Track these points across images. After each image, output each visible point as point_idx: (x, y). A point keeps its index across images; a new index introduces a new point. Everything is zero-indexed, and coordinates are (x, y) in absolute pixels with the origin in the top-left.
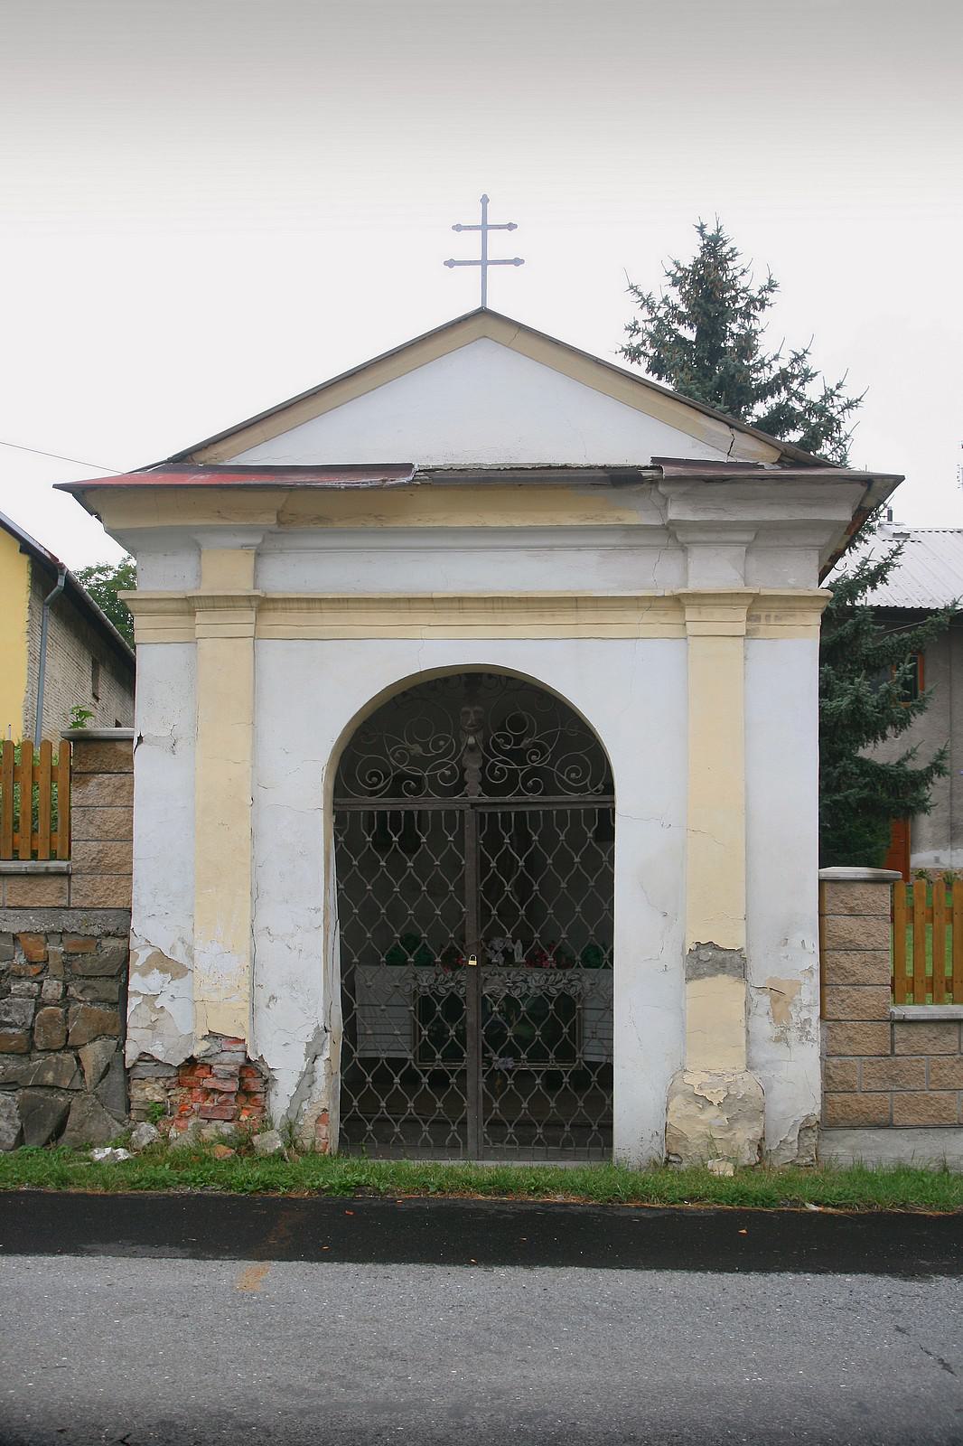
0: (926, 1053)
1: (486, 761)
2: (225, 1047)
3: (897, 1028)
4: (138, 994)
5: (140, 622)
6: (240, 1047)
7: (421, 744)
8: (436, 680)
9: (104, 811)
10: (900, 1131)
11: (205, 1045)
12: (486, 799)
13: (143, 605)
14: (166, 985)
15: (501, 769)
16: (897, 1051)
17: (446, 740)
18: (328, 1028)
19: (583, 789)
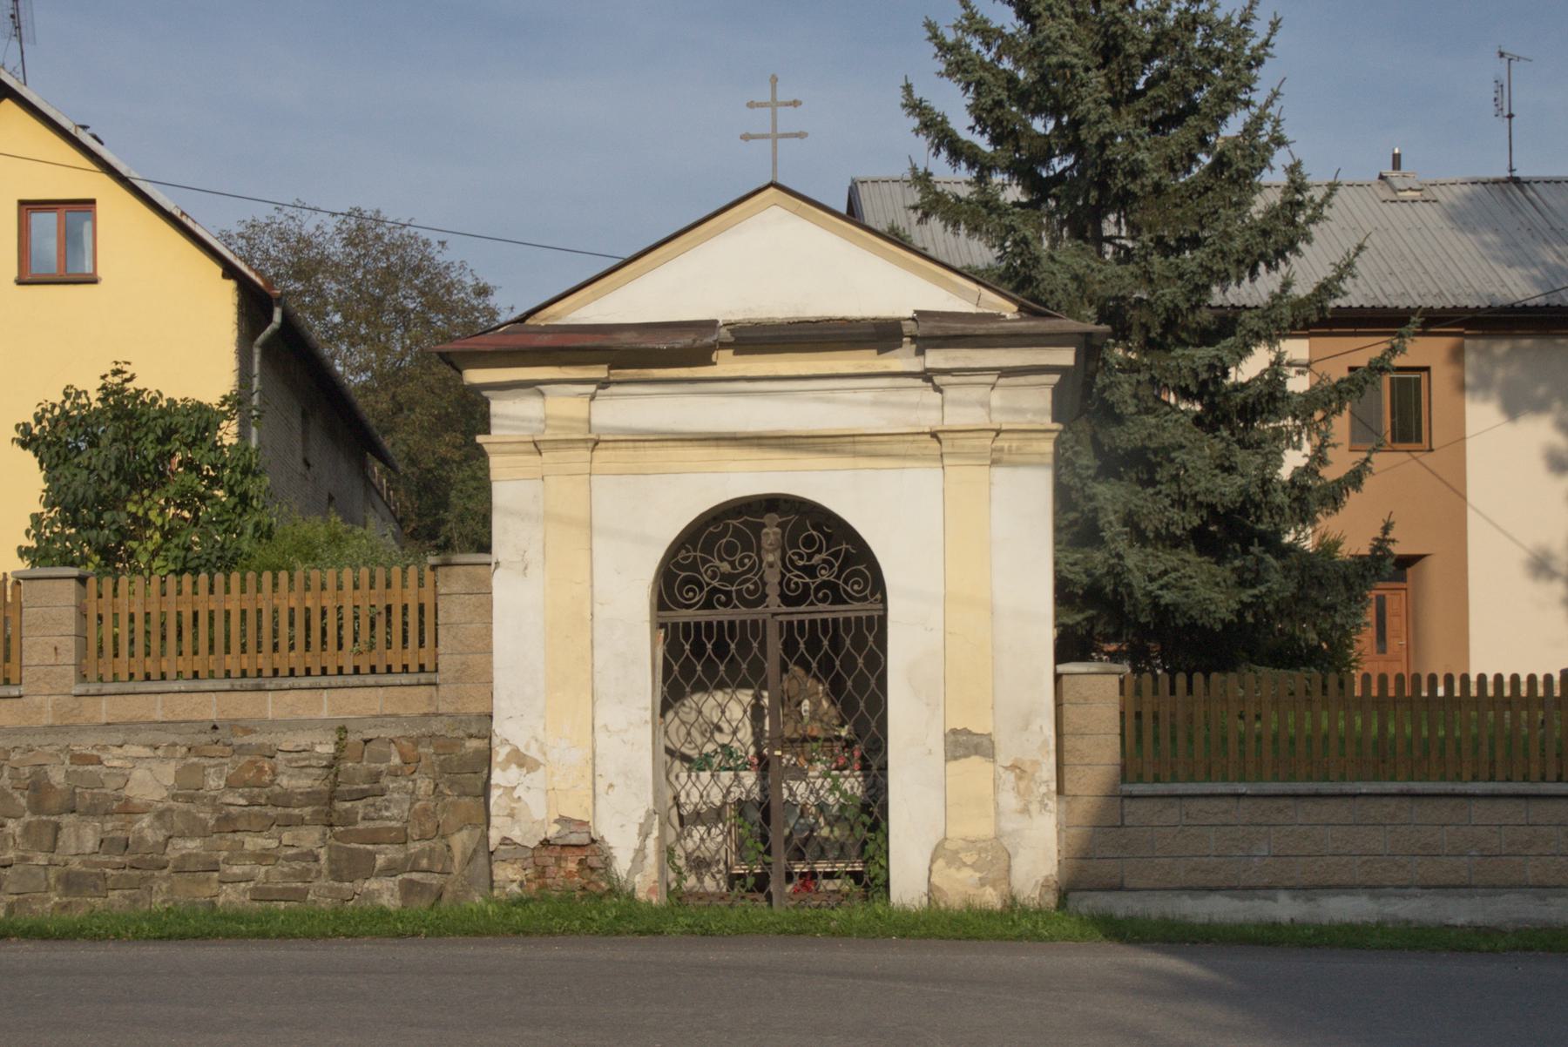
1: (783, 575)
2: (573, 828)
3: (1127, 802)
4: (498, 786)
6: (586, 829)
12: (784, 609)
13: (497, 447)
15: (796, 583)
16: (1126, 823)
17: (750, 557)
19: (865, 599)
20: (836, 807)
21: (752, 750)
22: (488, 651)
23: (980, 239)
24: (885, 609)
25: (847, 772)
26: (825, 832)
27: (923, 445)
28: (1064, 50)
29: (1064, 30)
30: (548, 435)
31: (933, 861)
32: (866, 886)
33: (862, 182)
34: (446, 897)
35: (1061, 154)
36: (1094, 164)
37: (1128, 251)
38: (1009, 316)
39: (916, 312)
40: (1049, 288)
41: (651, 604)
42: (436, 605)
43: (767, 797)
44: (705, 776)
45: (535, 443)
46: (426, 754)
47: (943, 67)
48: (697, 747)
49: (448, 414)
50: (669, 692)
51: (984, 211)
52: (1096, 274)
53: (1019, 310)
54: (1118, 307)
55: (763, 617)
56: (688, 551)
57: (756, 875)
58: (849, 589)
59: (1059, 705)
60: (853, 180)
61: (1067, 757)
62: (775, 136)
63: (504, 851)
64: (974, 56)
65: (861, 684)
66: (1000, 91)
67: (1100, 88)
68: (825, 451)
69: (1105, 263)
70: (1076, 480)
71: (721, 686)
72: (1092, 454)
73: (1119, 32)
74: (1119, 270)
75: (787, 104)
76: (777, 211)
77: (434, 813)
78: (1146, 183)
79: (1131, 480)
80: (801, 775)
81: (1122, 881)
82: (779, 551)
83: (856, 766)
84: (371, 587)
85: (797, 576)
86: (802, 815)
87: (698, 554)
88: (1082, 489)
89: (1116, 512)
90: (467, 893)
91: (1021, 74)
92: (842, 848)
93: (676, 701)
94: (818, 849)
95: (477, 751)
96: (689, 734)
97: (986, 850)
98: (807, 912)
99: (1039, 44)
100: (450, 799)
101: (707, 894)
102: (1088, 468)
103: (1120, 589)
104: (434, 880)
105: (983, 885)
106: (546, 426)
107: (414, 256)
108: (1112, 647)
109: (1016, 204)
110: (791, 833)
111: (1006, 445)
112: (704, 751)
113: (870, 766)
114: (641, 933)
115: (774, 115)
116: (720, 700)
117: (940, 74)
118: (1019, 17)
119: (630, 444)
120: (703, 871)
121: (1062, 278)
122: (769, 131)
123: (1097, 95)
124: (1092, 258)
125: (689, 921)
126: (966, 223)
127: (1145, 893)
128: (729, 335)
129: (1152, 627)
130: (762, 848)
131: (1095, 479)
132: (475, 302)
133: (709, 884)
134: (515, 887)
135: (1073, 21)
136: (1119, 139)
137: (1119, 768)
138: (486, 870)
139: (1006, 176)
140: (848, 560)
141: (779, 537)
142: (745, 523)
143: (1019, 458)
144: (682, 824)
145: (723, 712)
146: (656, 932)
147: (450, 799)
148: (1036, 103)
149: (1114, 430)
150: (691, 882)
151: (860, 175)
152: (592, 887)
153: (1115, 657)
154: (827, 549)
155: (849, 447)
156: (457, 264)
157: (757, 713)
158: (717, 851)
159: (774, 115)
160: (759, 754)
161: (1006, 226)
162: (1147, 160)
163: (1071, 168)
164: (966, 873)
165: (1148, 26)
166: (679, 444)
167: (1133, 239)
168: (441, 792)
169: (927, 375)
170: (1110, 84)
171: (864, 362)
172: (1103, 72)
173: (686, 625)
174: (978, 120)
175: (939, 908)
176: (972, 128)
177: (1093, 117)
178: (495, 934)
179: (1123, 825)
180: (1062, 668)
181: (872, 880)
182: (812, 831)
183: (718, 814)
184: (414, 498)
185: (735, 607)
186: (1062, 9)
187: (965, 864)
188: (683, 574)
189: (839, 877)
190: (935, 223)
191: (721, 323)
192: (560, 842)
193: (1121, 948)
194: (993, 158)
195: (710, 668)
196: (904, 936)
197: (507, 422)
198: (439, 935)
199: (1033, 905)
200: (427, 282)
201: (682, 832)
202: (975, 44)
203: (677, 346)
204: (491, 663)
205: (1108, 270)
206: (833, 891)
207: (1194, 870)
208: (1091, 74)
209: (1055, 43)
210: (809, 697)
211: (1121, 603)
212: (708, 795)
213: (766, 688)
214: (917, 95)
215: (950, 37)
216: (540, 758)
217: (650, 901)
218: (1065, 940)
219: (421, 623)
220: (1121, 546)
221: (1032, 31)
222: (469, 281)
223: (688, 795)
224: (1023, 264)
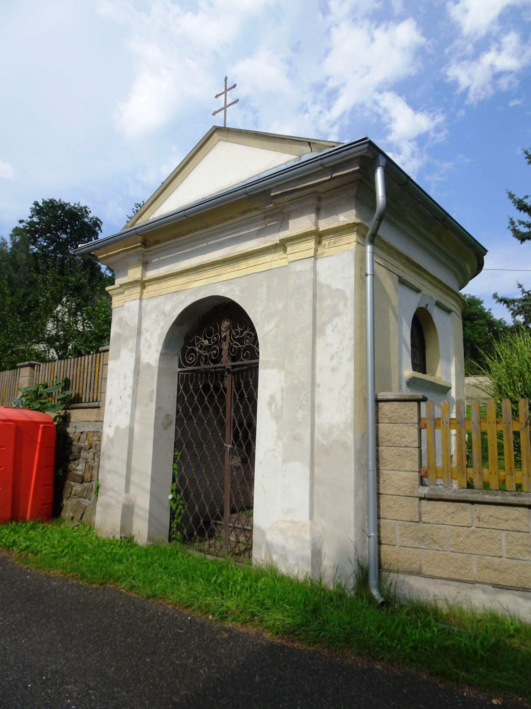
1: (230, 344)
3: (424, 502)
16: (423, 519)
76: (221, 143)
127: (439, 581)
207: (487, 567)
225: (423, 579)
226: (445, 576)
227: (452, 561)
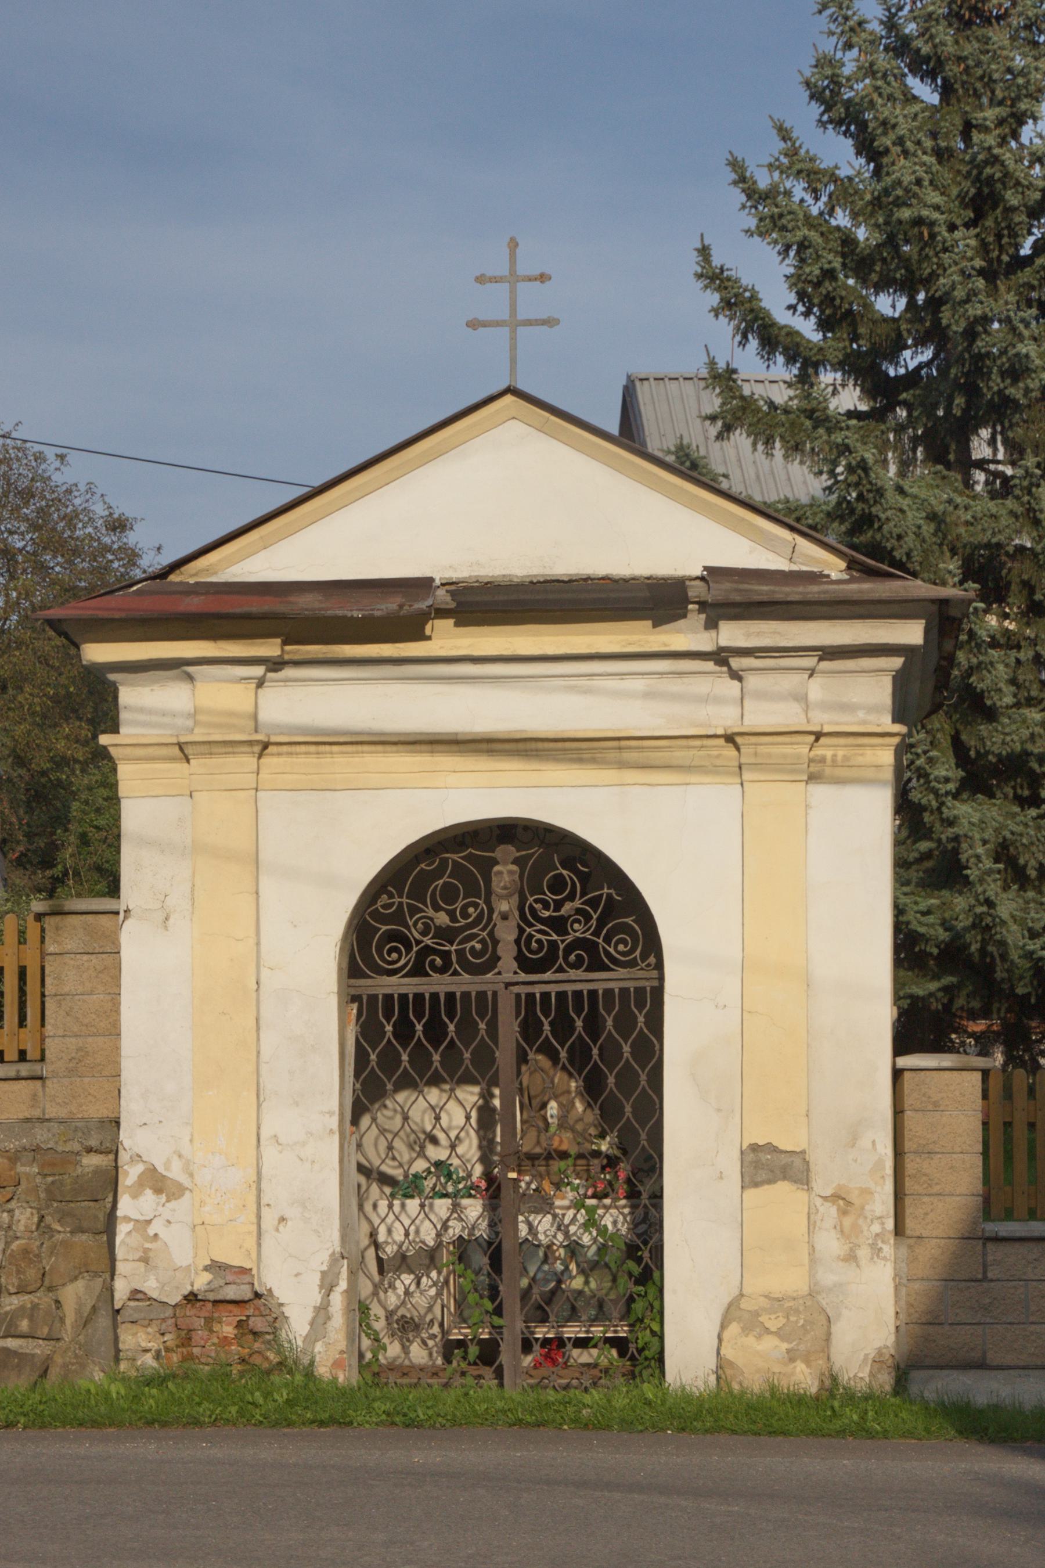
0: (1025, 1277)
1: (521, 931)
2: (230, 1278)
3: (991, 1247)
4: (127, 1219)
5: (124, 770)
6: (246, 1278)
7: (448, 912)
8: (463, 834)
9: (84, 1001)
10: (996, 1372)
11: (207, 1277)
12: (523, 977)
13: (128, 751)
14: (160, 1208)
15: (539, 941)
16: (990, 1275)
17: (476, 905)
18: (345, 1255)
19: (633, 964)
20: (594, 1248)
21: (478, 1170)
22: (114, 1032)
23: (802, 463)
24: (661, 978)
25: (607, 1201)
26: (577, 1283)
27: (715, 753)
28: (921, 201)
29: (921, 172)
30: (199, 735)
31: (723, 1327)
32: (633, 1358)
33: (641, 380)
34: (54, 1373)
35: (915, 345)
36: (960, 360)
37: (1006, 480)
38: (834, 575)
39: (706, 568)
40: (896, 531)
41: (340, 969)
42: (43, 968)
43: (497, 1234)
44: (413, 1204)
45: (181, 746)
46: (27, 1175)
47: (752, 223)
48: (401, 1165)
49: (69, 695)
50: (364, 1090)
51: (808, 423)
52: (961, 512)
53: (849, 568)
54: (991, 559)
55: (495, 987)
56: (391, 896)
57: (481, 1342)
58: (611, 950)
59: (898, 1112)
60: (629, 377)
61: (909, 1185)
62: (514, 323)
63: (136, 1309)
64: (795, 207)
65: (627, 1079)
66: (831, 257)
67: (969, 254)
68: (580, 760)
69: (974, 497)
70: (931, 796)
71: (435, 1081)
72: (953, 761)
73: (998, 175)
74: (992, 506)
75: (530, 279)
76: (516, 428)
77: (38, 1256)
78: (1031, 386)
79: (1006, 797)
80: (545, 1205)
81: (984, 1353)
82: (516, 897)
83: (621, 1192)
84: (848, 162)
85: (539, 931)
86: (546, 1260)
87: (405, 900)
88: (939, 809)
89: (985, 842)
90: (83, 1366)
91: (861, 234)
92: (601, 1305)
93: (372, 1102)
94: (567, 1306)
95: (98, 1171)
96: (390, 1148)
97: (797, 1312)
98: (551, 1396)
99: (886, 192)
100: (61, 1237)
101: (413, 1366)
102: (947, 780)
103: (990, 948)
104: (37, 1349)
105: (792, 1360)
106: (195, 723)
107: (23, 480)
108: (979, 1026)
109: (851, 414)
110: (530, 1286)
111: (829, 753)
112: (412, 1171)
113: (639, 1193)
114: (322, 1424)
115: (513, 292)
116: (433, 1102)
117: (749, 232)
118: (858, 153)
119: (313, 748)
120: (411, 1336)
121: (914, 517)
122: (505, 316)
123: (964, 263)
124: (956, 490)
125: (388, 1406)
126: (782, 438)
128: (449, 598)
129: (1033, 1001)
130: (489, 1306)
131: (956, 796)
132: (107, 540)
133: (418, 1354)
134: (149, 1360)
135: (933, 160)
136: (996, 325)
137: (980, 1199)
138: (111, 1335)
139: (839, 375)
140: (611, 910)
141: (516, 877)
142: (469, 858)
143: (840, 772)
144: (381, 1271)
145: (438, 1118)
146: (344, 1423)
147: (61, 1237)
148: (881, 273)
149: (984, 729)
150: (394, 1349)
151: (640, 369)
152: (257, 1360)
153: (984, 1044)
154: (583, 894)
155: (612, 755)
156: (82, 488)
157: (486, 1117)
158: (430, 1309)
159: (513, 292)
160: (488, 1176)
161: (838, 446)
162: (1033, 355)
163: (928, 364)
164: (769, 1344)
165: (1037, 167)
166: (380, 748)
167: (1013, 464)
168: (49, 1227)
169: (720, 657)
170: (984, 248)
171: (635, 638)
172: (973, 231)
173: (389, 998)
174: (801, 296)
175: (731, 1392)
176: (792, 308)
177: (959, 294)
178: (120, 1425)
179: (985, 1278)
180: (903, 1062)
181: (640, 1351)
182: (559, 1282)
183: (431, 1257)
184: (21, 812)
185: (455, 973)
186: (918, 143)
187: (767, 1331)
188: (384, 928)
189: (595, 1346)
190: (740, 439)
191: (438, 582)
192: (211, 1296)
193: (981, 1449)
194: (821, 349)
195: (420, 1059)
196: (683, 1429)
197: (142, 717)
198: (43, 1426)
199: (861, 1387)
200: (40, 511)
201: (381, 1282)
202: (799, 190)
203: (377, 613)
204: (118, 1048)
205: (978, 507)
206: (588, 1365)
208: (958, 234)
209: (907, 190)
210: (556, 1098)
211: (991, 968)
212: (417, 1232)
213: (497, 1085)
214: (716, 262)
215: (763, 181)
216: (183, 1179)
217: (336, 1378)
218: (903, 1436)
219: (22, 992)
220: (993, 888)
221: (877, 173)
222: (99, 510)
223: (389, 1231)
224: (860, 497)
225: (988, 1372)
226: (1022, 1363)
227: (1033, 1338)
